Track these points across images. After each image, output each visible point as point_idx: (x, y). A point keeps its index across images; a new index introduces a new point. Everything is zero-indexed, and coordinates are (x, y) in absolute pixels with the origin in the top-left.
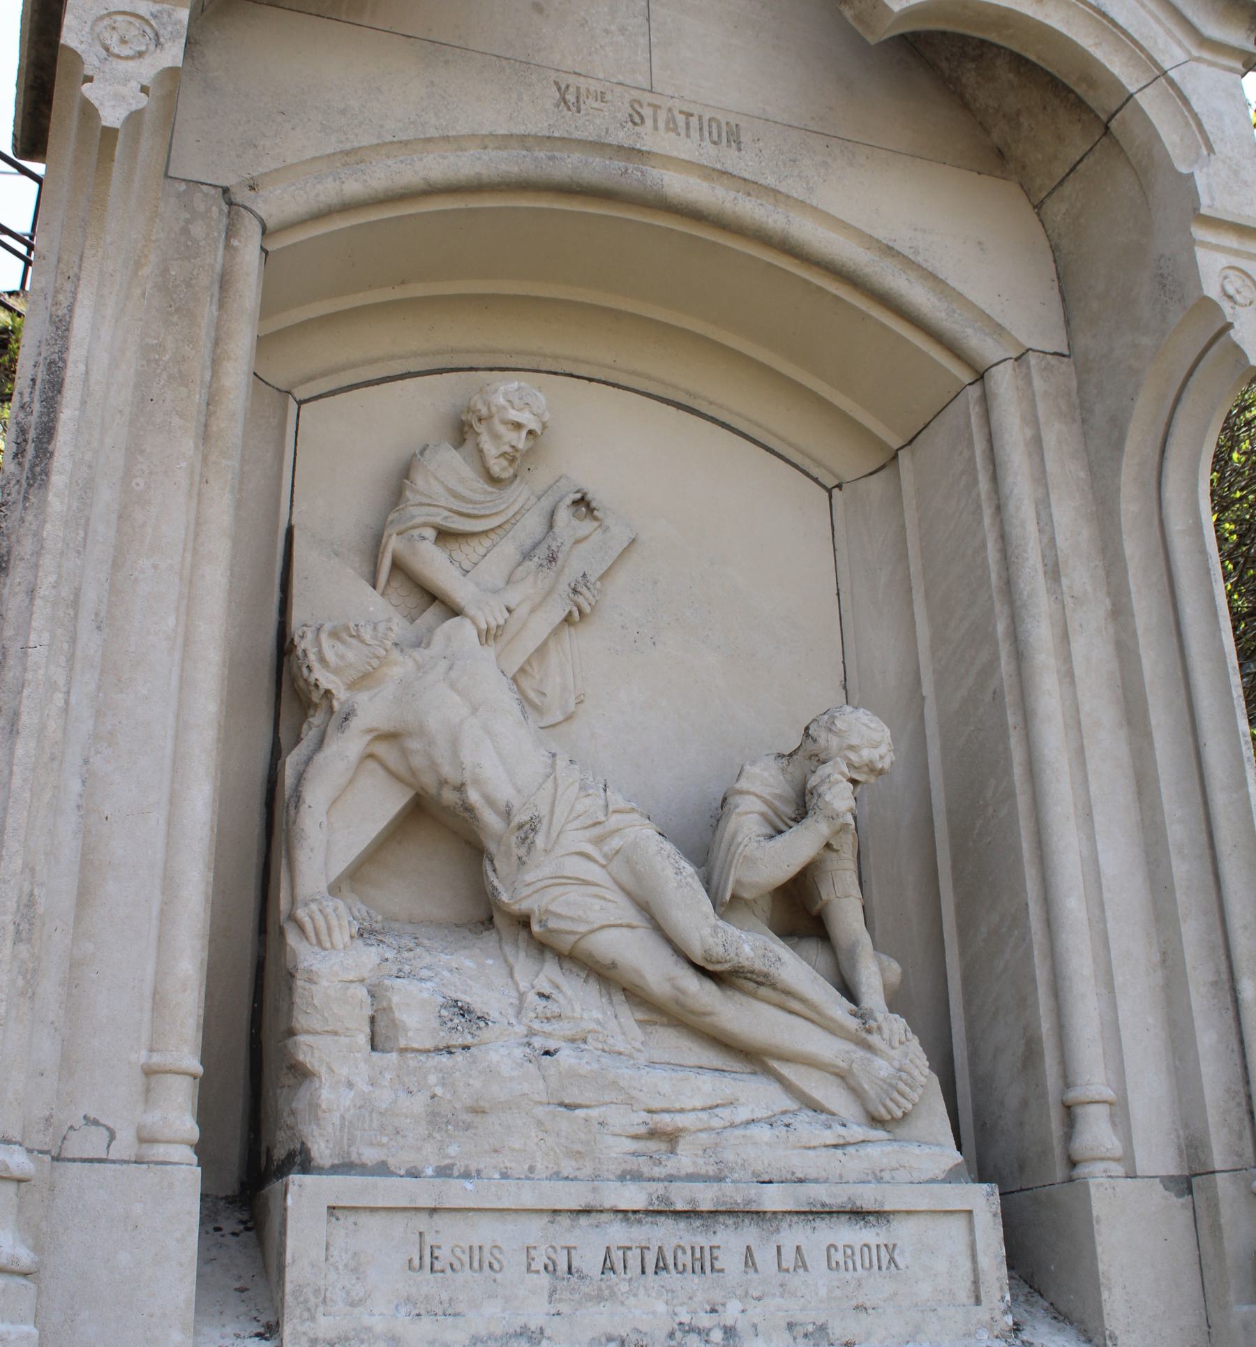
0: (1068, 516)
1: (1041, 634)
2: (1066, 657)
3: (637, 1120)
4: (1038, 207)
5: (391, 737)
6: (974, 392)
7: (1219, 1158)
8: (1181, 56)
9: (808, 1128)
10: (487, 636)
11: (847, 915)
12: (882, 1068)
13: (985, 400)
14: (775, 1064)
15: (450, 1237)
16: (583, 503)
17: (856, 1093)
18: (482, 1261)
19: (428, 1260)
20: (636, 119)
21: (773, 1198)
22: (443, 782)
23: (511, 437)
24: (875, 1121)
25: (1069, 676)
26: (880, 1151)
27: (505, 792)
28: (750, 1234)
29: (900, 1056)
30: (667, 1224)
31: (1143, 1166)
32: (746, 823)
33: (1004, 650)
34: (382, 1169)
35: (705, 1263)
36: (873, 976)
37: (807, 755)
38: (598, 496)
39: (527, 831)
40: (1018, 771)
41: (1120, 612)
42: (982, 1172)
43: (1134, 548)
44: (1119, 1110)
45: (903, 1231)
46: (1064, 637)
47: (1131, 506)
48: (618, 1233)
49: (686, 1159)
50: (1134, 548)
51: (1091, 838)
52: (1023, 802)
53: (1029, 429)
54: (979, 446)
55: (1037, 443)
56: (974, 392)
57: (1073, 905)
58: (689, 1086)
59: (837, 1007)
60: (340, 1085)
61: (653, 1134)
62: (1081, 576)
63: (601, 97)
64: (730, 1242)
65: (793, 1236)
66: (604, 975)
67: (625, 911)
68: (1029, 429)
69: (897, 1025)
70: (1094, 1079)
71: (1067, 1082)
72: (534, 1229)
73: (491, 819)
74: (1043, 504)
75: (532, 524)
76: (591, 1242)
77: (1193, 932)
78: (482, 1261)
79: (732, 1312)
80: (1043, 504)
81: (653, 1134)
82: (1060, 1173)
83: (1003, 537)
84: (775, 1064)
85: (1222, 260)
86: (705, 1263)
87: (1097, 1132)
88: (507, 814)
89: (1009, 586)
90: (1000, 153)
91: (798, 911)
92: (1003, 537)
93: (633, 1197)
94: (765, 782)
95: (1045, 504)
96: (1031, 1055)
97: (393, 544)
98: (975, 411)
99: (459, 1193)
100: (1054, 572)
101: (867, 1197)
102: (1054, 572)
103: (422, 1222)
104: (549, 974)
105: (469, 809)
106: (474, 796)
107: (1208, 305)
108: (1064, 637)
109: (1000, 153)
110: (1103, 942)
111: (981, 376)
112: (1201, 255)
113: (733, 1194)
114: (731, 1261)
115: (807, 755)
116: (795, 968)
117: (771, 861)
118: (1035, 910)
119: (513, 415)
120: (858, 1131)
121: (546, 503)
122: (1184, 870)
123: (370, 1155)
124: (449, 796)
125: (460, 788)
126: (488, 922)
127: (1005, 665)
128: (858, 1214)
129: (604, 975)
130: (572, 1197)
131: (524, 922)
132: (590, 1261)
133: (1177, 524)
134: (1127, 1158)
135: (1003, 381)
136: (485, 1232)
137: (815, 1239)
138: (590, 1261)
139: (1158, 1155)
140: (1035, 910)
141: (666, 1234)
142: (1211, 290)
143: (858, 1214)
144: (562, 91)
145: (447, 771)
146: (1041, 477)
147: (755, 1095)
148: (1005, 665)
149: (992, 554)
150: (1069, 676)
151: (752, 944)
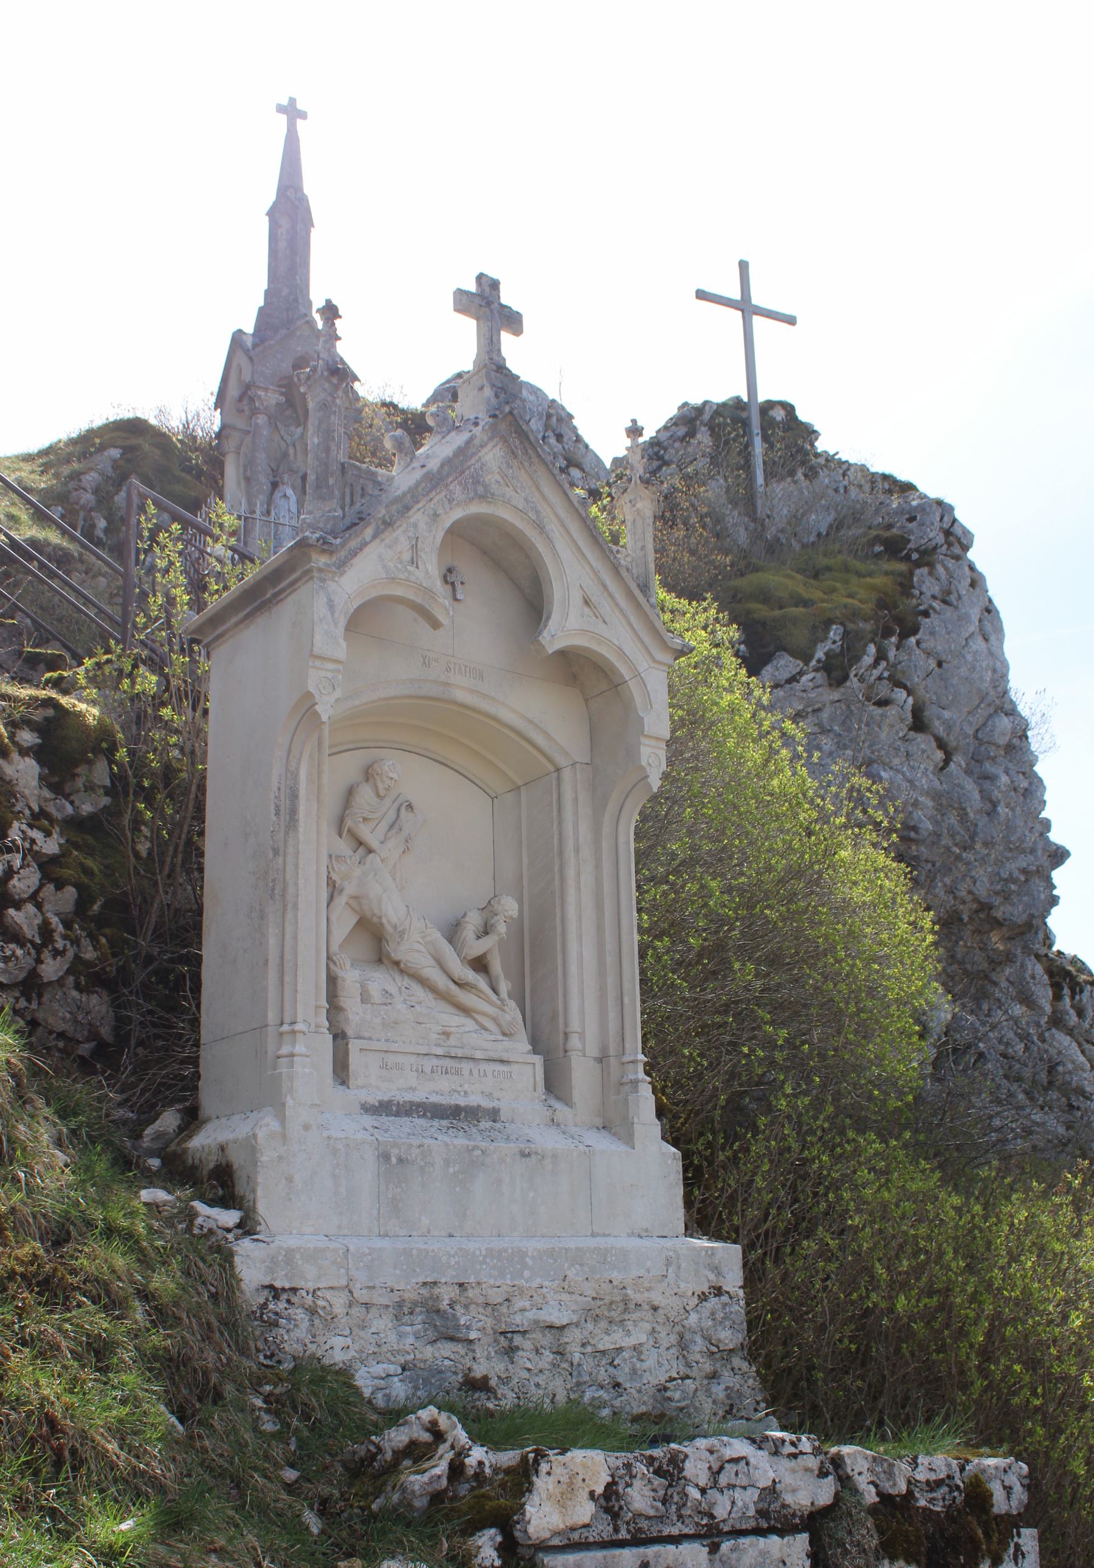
0: (584, 829)
1: (571, 873)
2: (578, 882)
3: (439, 1029)
4: (586, 701)
5: (356, 898)
6: (555, 775)
7: (612, 1052)
8: (646, 665)
9: (486, 1035)
10: (382, 861)
11: (496, 966)
12: (508, 1017)
13: (559, 779)
14: (477, 1017)
15: (391, 1059)
16: (410, 807)
17: (498, 1025)
18: (399, 1067)
19: (385, 1066)
20: (448, 670)
21: (478, 1055)
22: (374, 915)
23: (388, 782)
24: (504, 1034)
25: (578, 889)
26: (507, 1044)
27: (394, 920)
28: (471, 1065)
29: (512, 1013)
30: (448, 1060)
31: (588, 1052)
32: (469, 932)
33: (557, 876)
34: (370, 1039)
35: (458, 1072)
36: (504, 987)
37: (489, 909)
38: (414, 804)
39: (402, 934)
40: (558, 920)
41: (598, 867)
42: (535, 1052)
43: (606, 845)
44: (582, 1036)
45: (515, 1068)
46: (578, 875)
47: (606, 829)
48: (435, 1062)
49: (452, 1041)
50: (606, 845)
51: (581, 946)
52: (559, 930)
53: (574, 789)
54: (555, 797)
55: (576, 800)
56: (555, 775)
57: (573, 969)
58: (455, 1021)
59: (493, 997)
60: (355, 1012)
61: (444, 1033)
62: (586, 852)
63: (437, 661)
64: (466, 1066)
65: (484, 1066)
66: (423, 982)
67: (431, 962)
68: (574, 789)
69: (512, 1004)
70: (575, 1025)
71: (566, 1025)
72: (413, 1059)
73: (390, 929)
74: (576, 824)
75: (392, 815)
76: (428, 1064)
77: (611, 981)
78: (399, 1067)
79: (466, 1087)
80: (576, 824)
81: (444, 1033)
82: (561, 1054)
83: (560, 834)
84: (477, 1017)
85: (649, 750)
86: (458, 1072)
87: (575, 1042)
88: (395, 927)
89: (561, 853)
90: (575, 676)
91: (480, 965)
92: (560, 834)
93: (440, 1051)
94: (474, 920)
95: (577, 825)
96: (554, 1017)
97: (349, 823)
98: (554, 783)
99: (394, 1047)
100: (577, 850)
101: (505, 1056)
102: (577, 850)
103: (383, 1055)
104: (407, 981)
105: (382, 924)
106: (384, 920)
107: (644, 769)
108: (578, 875)
109: (575, 676)
110: (582, 981)
111: (558, 770)
112: (642, 748)
113: (467, 1052)
114: (466, 1072)
115: (489, 909)
116: (481, 982)
117: (477, 948)
118: (560, 968)
119: (391, 775)
120: (500, 1037)
121: (396, 804)
122: (610, 960)
123: (367, 1035)
124: (375, 919)
125: (380, 918)
126: (380, 961)
127: (557, 883)
128: (502, 1061)
129: (423, 982)
130: (423, 1050)
131: (397, 963)
132: (428, 1070)
133: (622, 840)
134: (583, 1051)
135: (567, 774)
136: (400, 1059)
137: (489, 1067)
138: (428, 1070)
139: (593, 1051)
140: (560, 968)
141: (448, 1063)
142: (644, 763)
143: (502, 1061)
144: (424, 658)
145: (376, 911)
146: (576, 813)
147: (470, 1025)
148: (557, 883)
149: (556, 840)
150: (578, 889)
151: (470, 975)
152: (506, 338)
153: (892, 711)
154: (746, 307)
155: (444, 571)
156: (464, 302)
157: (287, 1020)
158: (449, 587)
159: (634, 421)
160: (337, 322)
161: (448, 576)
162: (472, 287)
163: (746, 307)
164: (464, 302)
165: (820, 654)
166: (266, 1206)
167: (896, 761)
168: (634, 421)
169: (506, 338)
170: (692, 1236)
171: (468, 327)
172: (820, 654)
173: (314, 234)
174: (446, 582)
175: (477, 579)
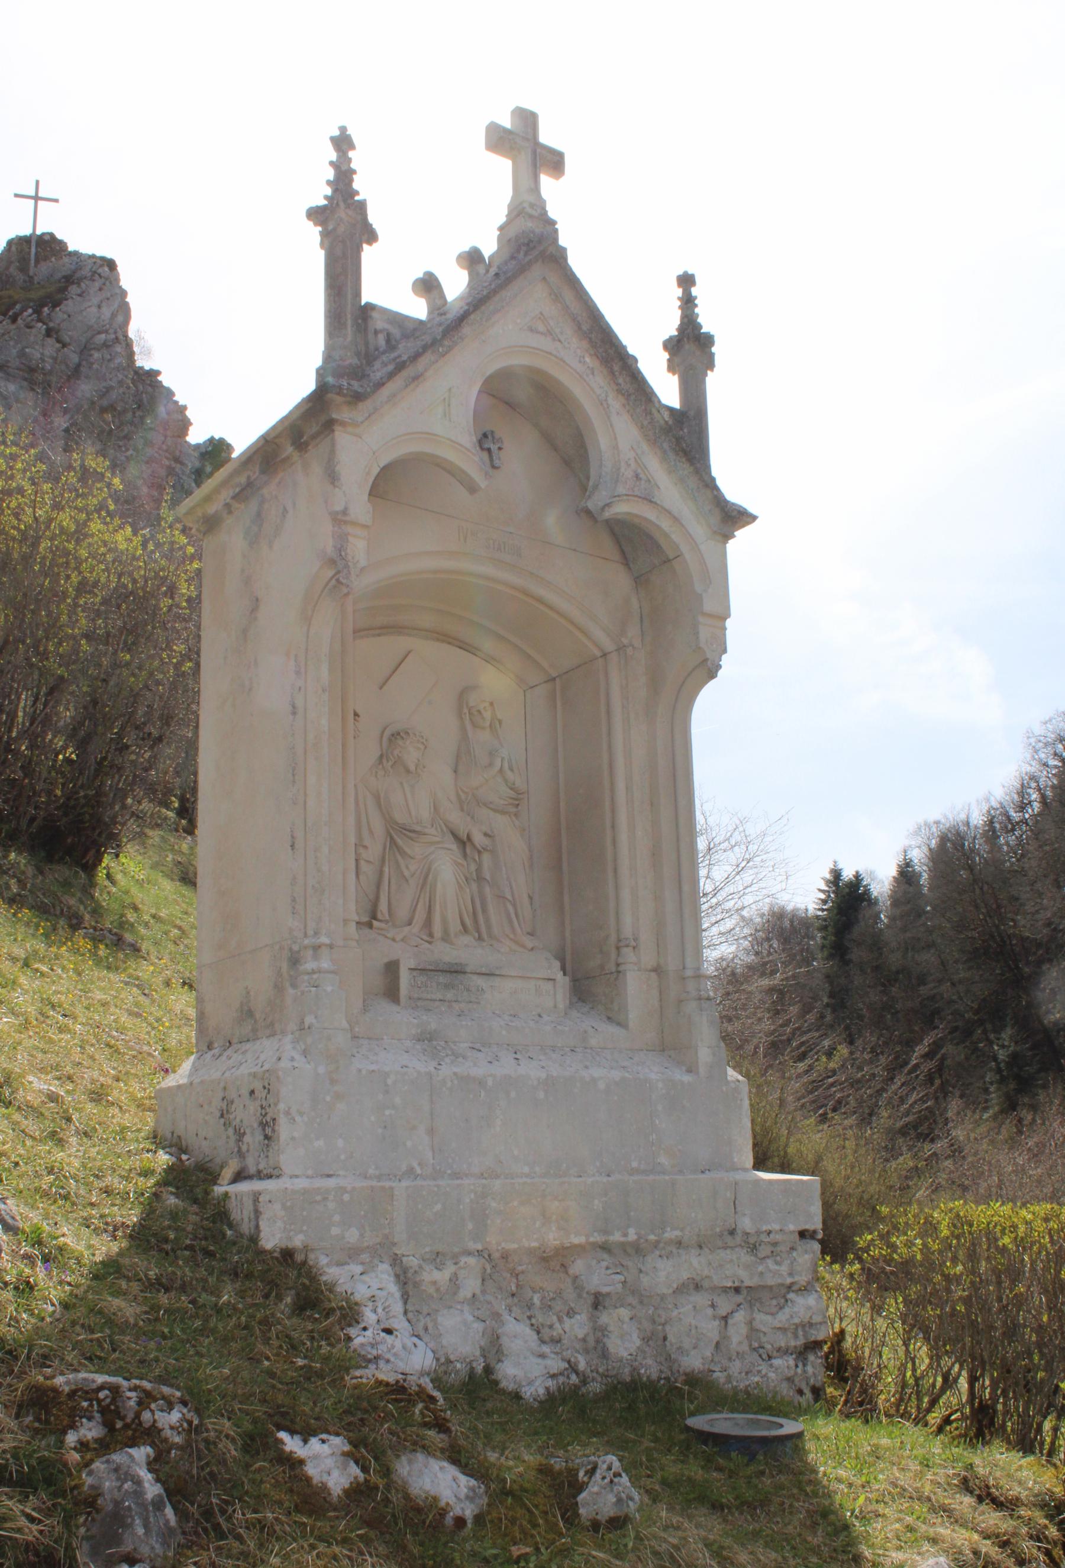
40: (607, 804)
152: (547, 183)
153: (34, 331)
154: (36, 198)
155: (480, 436)
156: (500, 140)
157: (310, 932)
158: (485, 455)
159: (343, 129)
160: (351, 154)
161: (486, 441)
162: (506, 122)
163: (36, 198)
164: (500, 140)
165: (11, 313)
166: (283, 1167)
167: (37, 347)
168: (343, 129)
169: (547, 183)
170: (758, 1170)
171: (502, 167)
172: (11, 313)
173: (640, 365)
174: (482, 449)
175: (522, 457)
